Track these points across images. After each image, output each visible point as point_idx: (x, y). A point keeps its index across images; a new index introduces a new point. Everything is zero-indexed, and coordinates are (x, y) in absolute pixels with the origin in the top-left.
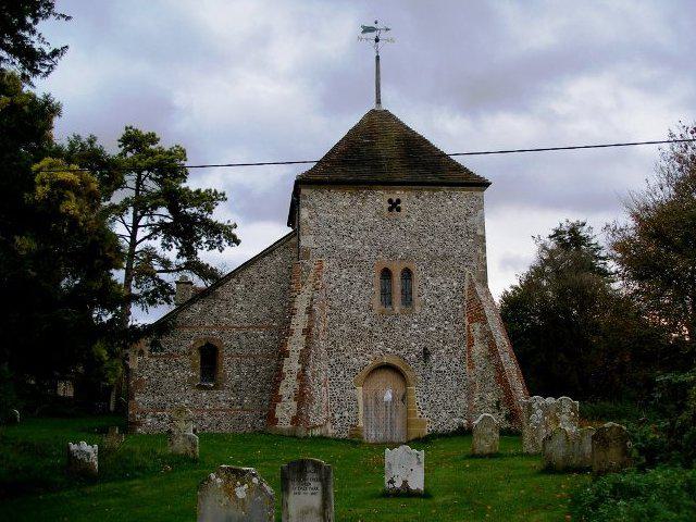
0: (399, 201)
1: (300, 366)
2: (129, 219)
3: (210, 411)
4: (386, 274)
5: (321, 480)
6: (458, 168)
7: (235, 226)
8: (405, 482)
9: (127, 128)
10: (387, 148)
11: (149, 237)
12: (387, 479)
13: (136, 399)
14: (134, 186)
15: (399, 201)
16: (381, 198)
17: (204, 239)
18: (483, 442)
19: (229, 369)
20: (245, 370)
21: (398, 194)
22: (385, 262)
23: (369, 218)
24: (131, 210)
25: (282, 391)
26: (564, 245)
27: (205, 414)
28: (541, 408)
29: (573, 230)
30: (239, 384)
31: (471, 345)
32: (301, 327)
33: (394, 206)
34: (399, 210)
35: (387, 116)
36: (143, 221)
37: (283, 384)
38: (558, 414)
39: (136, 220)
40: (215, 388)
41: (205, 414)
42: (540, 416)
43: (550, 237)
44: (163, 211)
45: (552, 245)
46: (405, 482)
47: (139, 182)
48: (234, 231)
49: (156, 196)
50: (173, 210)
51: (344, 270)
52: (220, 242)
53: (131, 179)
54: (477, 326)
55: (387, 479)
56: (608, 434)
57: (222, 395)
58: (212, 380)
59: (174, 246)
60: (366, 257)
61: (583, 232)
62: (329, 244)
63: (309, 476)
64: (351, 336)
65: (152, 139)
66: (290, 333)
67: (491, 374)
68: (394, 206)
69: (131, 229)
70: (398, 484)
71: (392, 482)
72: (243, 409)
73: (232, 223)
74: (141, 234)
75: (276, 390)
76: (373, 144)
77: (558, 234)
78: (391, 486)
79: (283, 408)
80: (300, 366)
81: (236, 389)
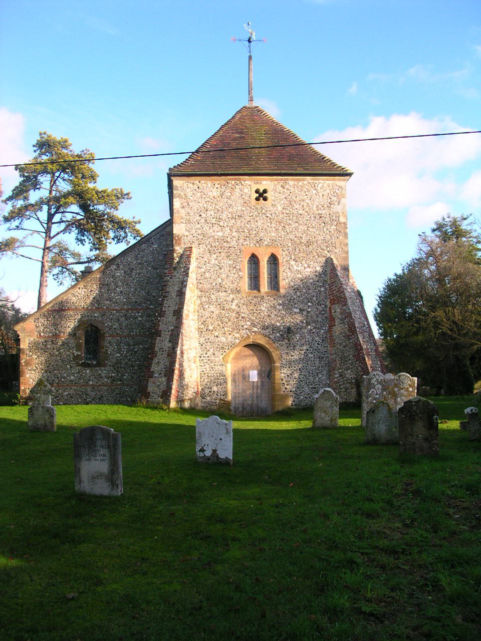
0: (265, 191)
1: (170, 345)
2: (43, 215)
3: (93, 387)
4: (254, 260)
5: (109, 447)
6: (322, 159)
7: (139, 222)
8: (214, 451)
9: (41, 134)
10: (260, 138)
11: (64, 231)
12: (198, 448)
13: (28, 376)
14: (48, 187)
15: (265, 191)
16: (250, 185)
17: (112, 234)
18: (323, 415)
19: (110, 346)
20: (124, 348)
21: (265, 183)
22: (251, 247)
23: (238, 208)
24: (45, 208)
25: (155, 368)
26: (445, 237)
27: (89, 389)
28: (379, 383)
29: (454, 223)
30: (118, 362)
31: (331, 327)
32: (172, 309)
33: (262, 195)
34: (265, 199)
35: (258, 111)
36: (57, 218)
37: (155, 360)
38: (396, 389)
39: (50, 217)
40: (99, 365)
41: (89, 389)
42: (379, 392)
43: (434, 230)
44: (75, 208)
45: (431, 236)
46: (214, 451)
47: (53, 182)
48: (138, 227)
49: (66, 195)
50: (84, 207)
51: (214, 256)
52: (126, 236)
53: (45, 180)
54: (337, 309)
55: (198, 448)
56: (415, 408)
57: (103, 372)
58: (95, 358)
59: (87, 240)
60: (234, 243)
61: (464, 226)
62: (200, 232)
63: (99, 443)
64: (220, 317)
65: (64, 144)
66: (162, 314)
67: (350, 353)
68: (262, 195)
69: (45, 226)
70: (208, 453)
71: (202, 450)
72: (123, 384)
73: (136, 220)
74: (55, 229)
75: (148, 367)
76: (243, 138)
77: (440, 227)
78: (202, 454)
79: (154, 383)
80: (170, 345)
81: (117, 366)
